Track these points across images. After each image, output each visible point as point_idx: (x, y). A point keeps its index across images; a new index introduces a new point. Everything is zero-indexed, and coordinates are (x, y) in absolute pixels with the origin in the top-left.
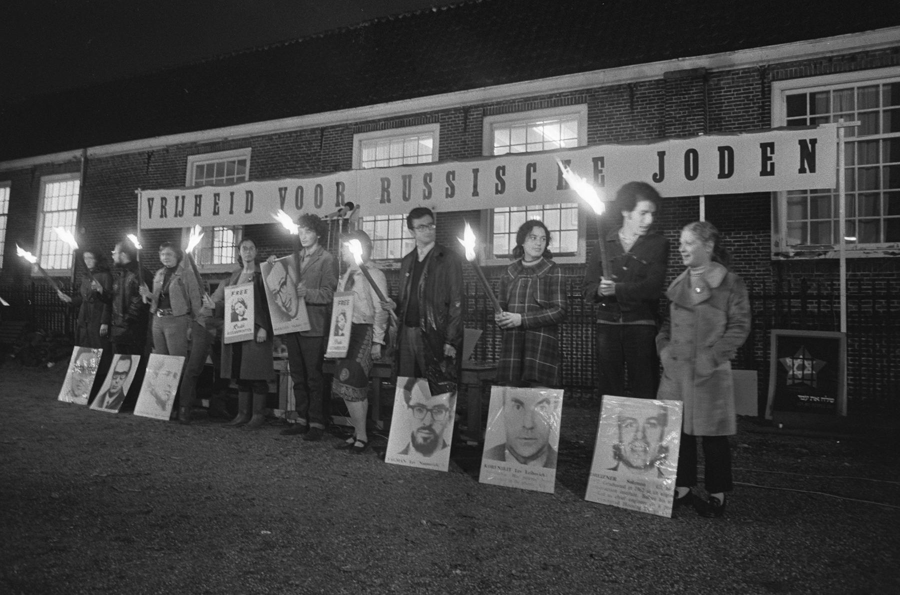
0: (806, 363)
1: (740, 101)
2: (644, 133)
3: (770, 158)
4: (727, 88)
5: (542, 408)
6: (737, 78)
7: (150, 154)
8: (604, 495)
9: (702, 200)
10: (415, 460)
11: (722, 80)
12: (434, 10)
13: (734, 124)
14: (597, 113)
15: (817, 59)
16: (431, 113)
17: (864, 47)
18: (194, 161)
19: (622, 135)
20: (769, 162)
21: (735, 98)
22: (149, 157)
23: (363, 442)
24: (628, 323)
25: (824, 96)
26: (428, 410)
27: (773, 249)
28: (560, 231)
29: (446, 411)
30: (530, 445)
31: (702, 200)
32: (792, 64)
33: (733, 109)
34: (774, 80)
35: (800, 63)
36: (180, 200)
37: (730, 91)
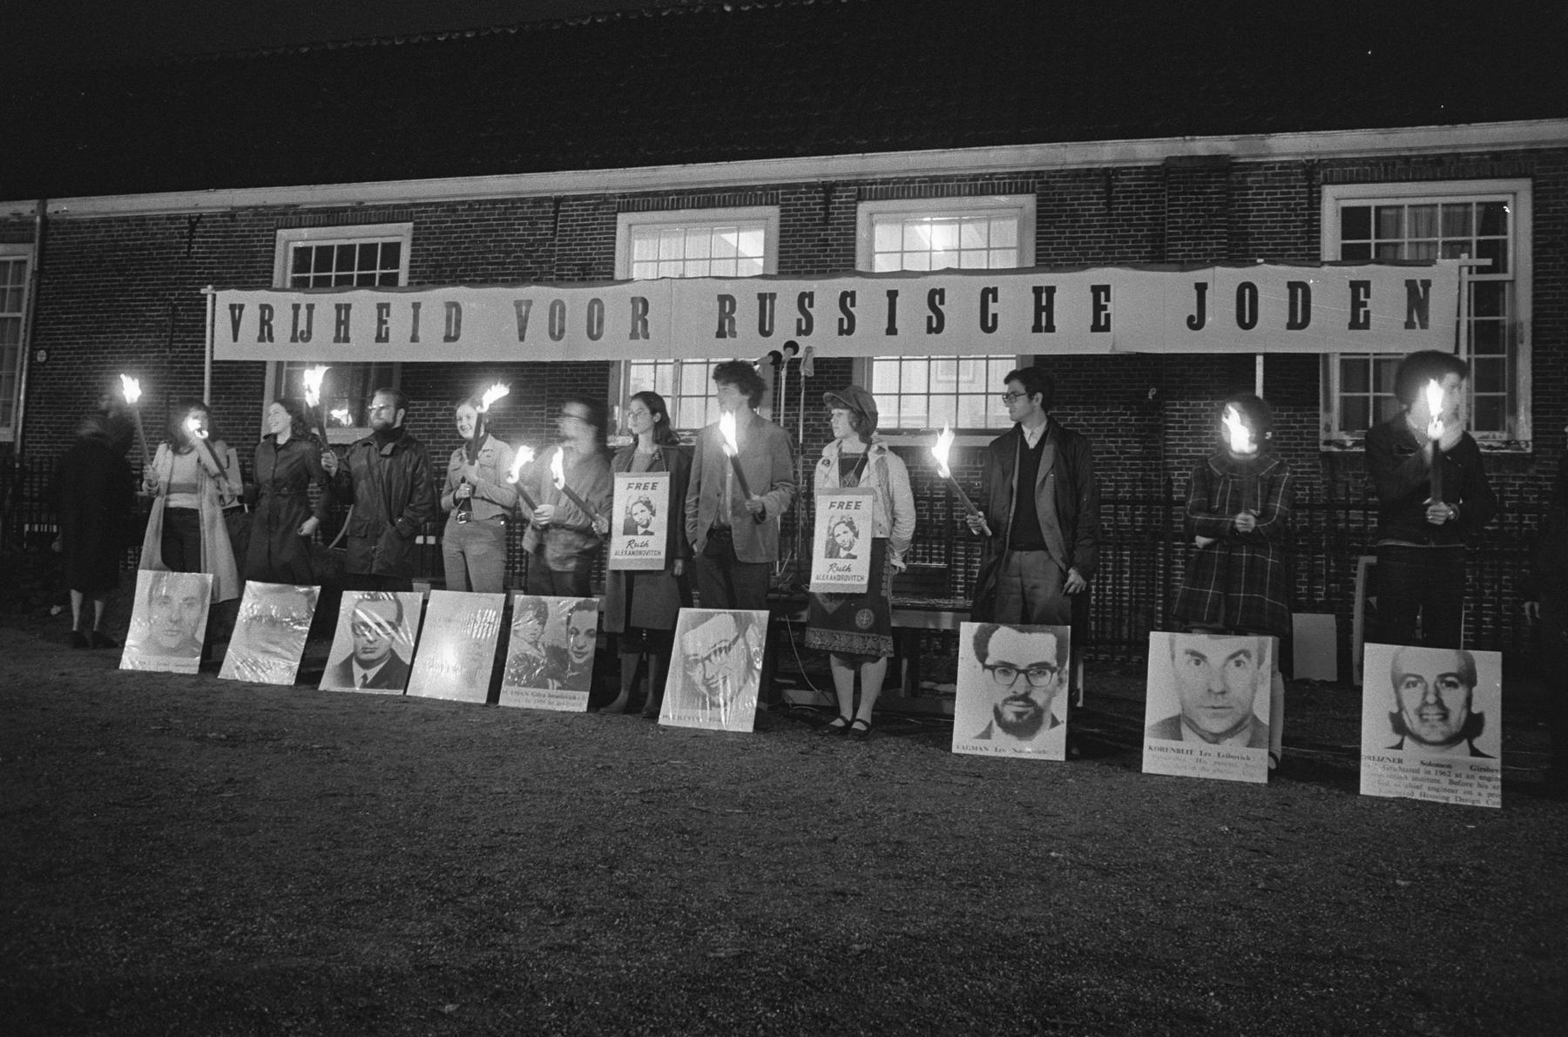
1: (1275, 210)
2: (1127, 247)
4: (1257, 188)
7: (195, 221)
9: (1260, 360)
10: (1005, 746)
11: (1250, 175)
12: (728, 9)
13: (1267, 244)
14: (1052, 211)
16: (765, 188)
17: (1455, 147)
18: (290, 239)
19: (1093, 248)
20: (1103, 313)
22: (193, 227)
23: (865, 723)
25: (1393, 212)
26: (1019, 672)
27: (1323, 436)
28: (957, 394)
29: (1052, 672)
30: (1223, 717)
31: (1260, 360)
32: (1353, 162)
34: (1326, 182)
35: (1365, 161)
36: (303, 312)
37: (1261, 194)
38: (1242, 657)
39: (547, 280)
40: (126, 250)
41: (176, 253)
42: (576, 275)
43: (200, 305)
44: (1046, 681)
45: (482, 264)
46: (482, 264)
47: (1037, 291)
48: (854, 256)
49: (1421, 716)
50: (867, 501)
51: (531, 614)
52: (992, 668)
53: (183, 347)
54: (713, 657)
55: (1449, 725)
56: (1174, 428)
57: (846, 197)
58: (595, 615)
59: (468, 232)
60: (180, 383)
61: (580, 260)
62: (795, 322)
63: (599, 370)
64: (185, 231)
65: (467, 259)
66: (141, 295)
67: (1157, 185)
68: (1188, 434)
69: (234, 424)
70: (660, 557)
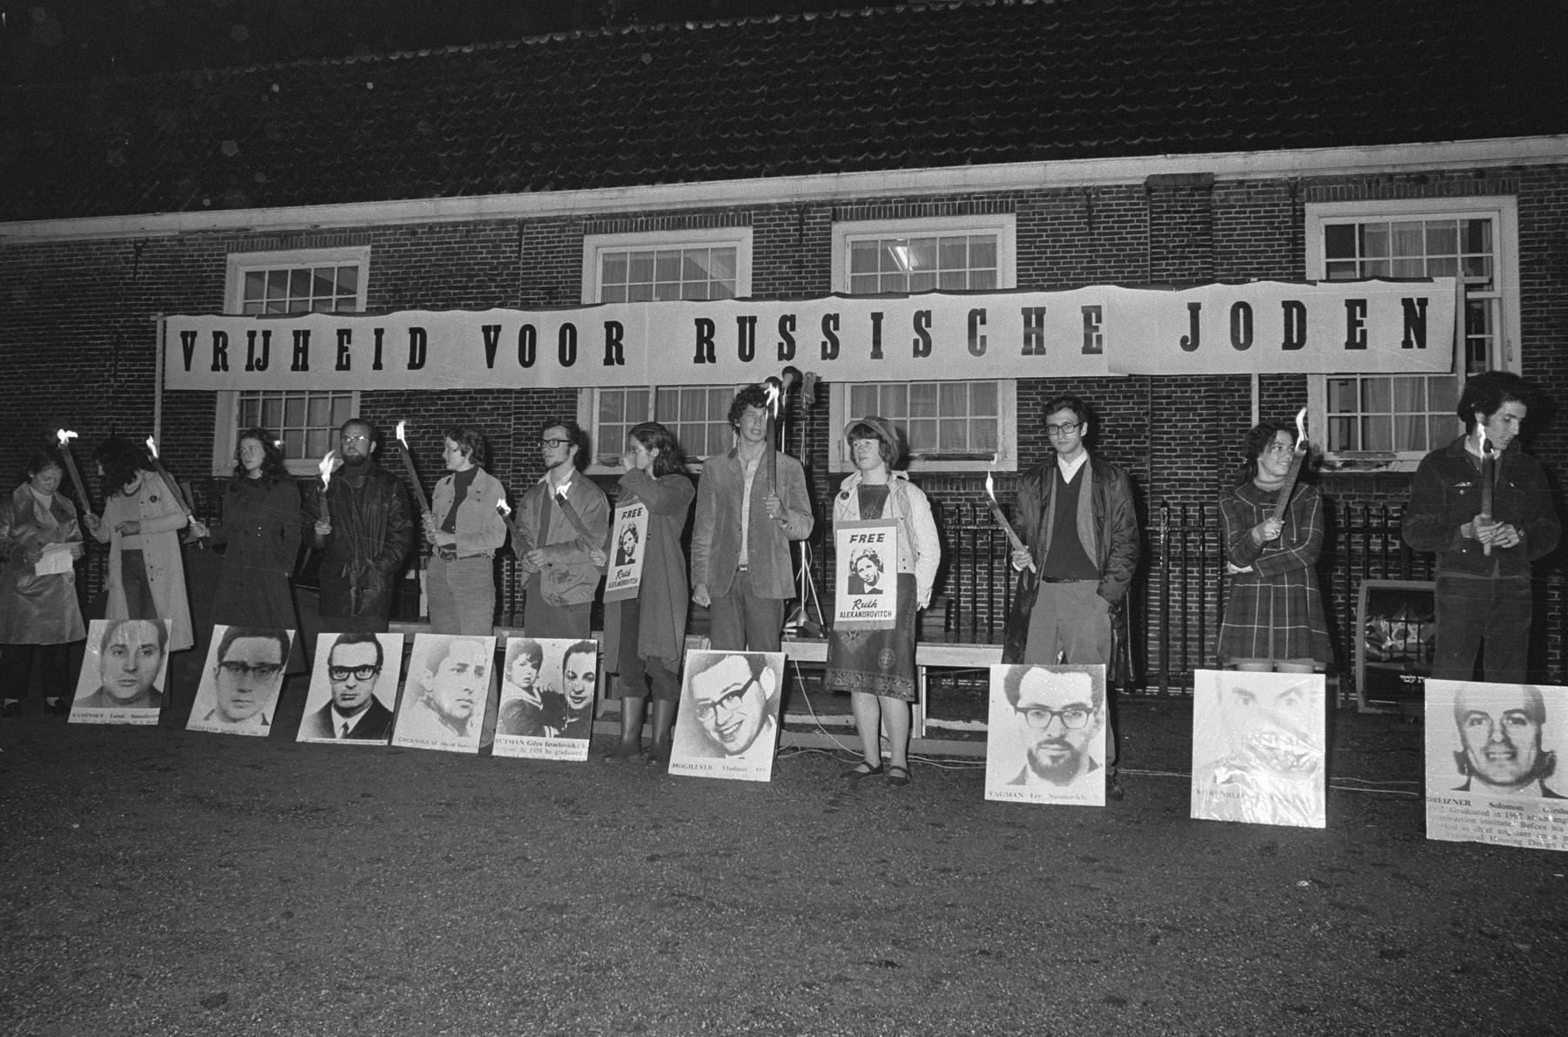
0: (1410, 627)
1: (1260, 228)
2: (1110, 267)
3: (1361, 323)
4: (1240, 207)
5: (1290, 702)
6: (1255, 193)
8: (1455, 828)
10: (1042, 792)
13: (1251, 263)
14: (1033, 231)
15: (1372, 175)
16: (736, 209)
19: (1075, 268)
20: (1358, 329)
21: (1251, 223)
22: (138, 251)
24: (1506, 577)
26: (1053, 714)
32: (1336, 179)
33: (1250, 240)
35: (1348, 179)
36: (259, 340)
37: (1245, 212)
38: (1293, 695)
39: (511, 304)
40: (68, 276)
41: (121, 279)
42: (542, 299)
43: (147, 332)
44: (1081, 723)
45: (444, 288)
46: (444, 288)
47: (1027, 312)
48: (829, 277)
49: (1487, 755)
50: (890, 532)
51: (523, 657)
52: (1025, 711)
53: (129, 376)
54: (725, 702)
55: (1518, 764)
56: (1162, 450)
57: (821, 218)
58: (593, 656)
59: (428, 255)
60: (125, 414)
61: (545, 283)
62: (912, 343)
63: (567, 397)
64: (130, 256)
65: (428, 283)
66: (83, 323)
67: (1138, 204)
68: (1176, 457)
69: (184, 456)
70: (888, 618)
